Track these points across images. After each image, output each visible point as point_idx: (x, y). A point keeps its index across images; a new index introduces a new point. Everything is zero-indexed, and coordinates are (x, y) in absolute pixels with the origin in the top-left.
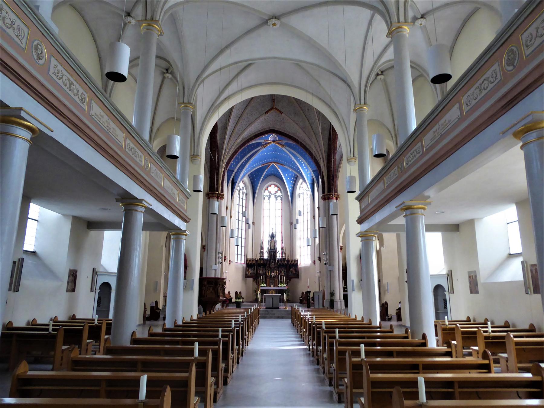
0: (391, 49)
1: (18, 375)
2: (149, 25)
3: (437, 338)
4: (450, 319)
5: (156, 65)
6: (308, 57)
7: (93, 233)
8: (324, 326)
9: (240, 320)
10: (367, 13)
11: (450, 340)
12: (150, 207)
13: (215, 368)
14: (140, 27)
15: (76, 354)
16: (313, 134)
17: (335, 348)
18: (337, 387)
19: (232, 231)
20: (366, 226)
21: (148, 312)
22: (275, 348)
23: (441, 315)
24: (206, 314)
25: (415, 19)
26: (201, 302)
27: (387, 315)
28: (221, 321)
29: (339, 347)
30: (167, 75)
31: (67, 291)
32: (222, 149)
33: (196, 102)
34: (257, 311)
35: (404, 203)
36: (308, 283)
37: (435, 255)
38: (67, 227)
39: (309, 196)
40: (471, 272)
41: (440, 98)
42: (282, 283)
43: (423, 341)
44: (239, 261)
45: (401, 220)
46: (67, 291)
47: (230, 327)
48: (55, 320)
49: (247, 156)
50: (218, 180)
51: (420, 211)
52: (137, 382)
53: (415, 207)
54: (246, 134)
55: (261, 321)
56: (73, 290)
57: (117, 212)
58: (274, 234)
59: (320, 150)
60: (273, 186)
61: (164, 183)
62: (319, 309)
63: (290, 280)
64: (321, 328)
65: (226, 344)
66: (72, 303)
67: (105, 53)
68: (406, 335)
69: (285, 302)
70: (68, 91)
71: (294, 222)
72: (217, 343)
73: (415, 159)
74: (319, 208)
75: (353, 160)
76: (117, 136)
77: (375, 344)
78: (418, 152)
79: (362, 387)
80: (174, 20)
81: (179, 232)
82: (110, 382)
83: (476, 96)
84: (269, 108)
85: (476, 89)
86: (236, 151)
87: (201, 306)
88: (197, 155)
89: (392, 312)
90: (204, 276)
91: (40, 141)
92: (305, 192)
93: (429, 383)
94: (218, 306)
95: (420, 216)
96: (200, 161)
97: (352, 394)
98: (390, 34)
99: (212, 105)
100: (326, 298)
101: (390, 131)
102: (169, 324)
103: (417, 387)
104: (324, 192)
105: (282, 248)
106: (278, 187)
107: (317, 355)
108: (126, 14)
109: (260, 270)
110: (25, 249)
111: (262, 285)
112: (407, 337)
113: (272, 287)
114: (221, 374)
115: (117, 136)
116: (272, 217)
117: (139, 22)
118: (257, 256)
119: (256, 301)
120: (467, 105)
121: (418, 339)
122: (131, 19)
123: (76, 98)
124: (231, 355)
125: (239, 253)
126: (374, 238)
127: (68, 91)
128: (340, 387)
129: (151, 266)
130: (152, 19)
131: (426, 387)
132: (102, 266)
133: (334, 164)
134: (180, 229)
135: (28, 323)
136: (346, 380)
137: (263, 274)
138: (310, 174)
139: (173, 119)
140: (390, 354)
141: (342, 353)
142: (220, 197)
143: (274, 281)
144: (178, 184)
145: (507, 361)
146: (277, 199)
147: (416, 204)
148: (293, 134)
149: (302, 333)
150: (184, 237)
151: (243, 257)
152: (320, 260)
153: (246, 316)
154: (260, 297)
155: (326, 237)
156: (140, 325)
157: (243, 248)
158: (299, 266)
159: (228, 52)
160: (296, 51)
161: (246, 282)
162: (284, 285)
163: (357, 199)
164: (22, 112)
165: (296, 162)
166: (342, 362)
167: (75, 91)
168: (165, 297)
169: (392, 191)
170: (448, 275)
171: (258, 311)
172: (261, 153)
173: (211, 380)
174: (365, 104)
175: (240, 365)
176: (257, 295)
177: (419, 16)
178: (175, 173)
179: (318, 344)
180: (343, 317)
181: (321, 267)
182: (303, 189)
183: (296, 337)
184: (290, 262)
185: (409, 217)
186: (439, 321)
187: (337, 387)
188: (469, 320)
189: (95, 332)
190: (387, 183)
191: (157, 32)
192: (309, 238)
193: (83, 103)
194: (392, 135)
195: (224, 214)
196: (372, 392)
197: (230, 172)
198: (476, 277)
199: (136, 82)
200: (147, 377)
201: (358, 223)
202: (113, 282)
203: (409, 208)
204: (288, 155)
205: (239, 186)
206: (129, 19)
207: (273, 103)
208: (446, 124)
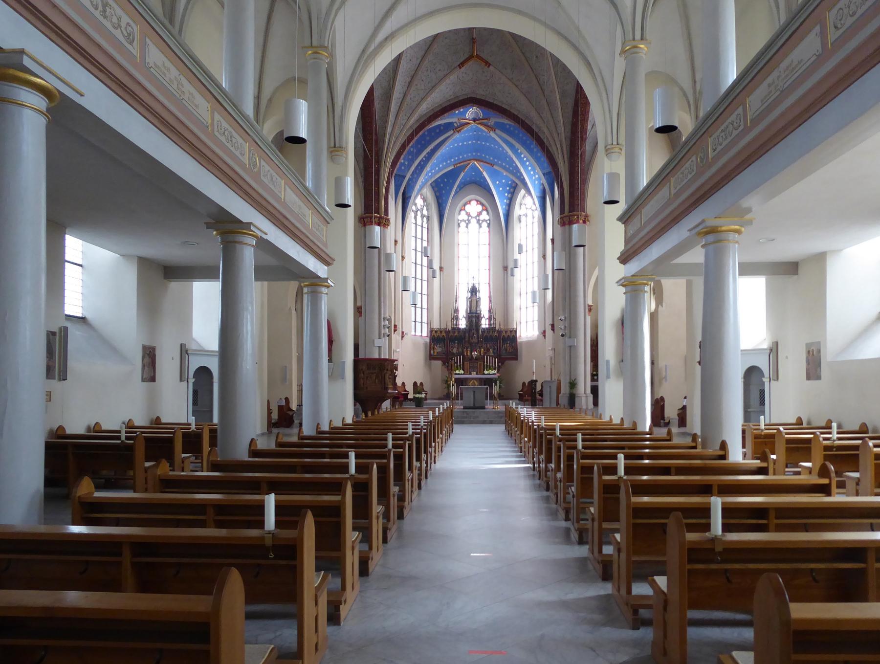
1: (79, 497)
4: (767, 422)
7: (175, 286)
8: (558, 432)
9: (422, 424)
12: (264, 236)
15: (164, 469)
18: (578, 522)
19: (405, 279)
20: (634, 267)
21: (275, 416)
22: (479, 475)
23: (753, 416)
24: (366, 416)
26: (358, 398)
27: (663, 418)
28: (393, 425)
29: (581, 461)
31: (143, 380)
33: (333, 45)
34: (449, 411)
35: (703, 221)
36: (532, 368)
37: (751, 314)
38: (130, 276)
39: (536, 219)
40: (812, 344)
41: (783, 19)
43: (722, 453)
44: (418, 333)
46: (143, 380)
47: (407, 433)
48: (130, 425)
49: (428, 150)
50: (378, 193)
51: (731, 236)
52: (260, 508)
53: (724, 228)
54: (425, 108)
55: (456, 427)
56: (153, 379)
57: (209, 248)
58: (477, 286)
60: (474, 203)
61: (287, 197)
62: (550, 408)
63: (503, 363)
65: (399, 458)
66: (152, 400)
68: (694, 444)
70: (101, 18)
71: (511, 265)
72: (385, 456)
73: (730, 139)
74: (553, 240)
75: (617, 150)
77: (641, 457)
81: (315, 282)
82: (219, 508)
84: (467, 56)
86: (409, 140)
88: (341, 147)
89: (671, 412)
90: (361, 356)
91: (64, 114)
92: (530, 213)
93: (727, 511)
94: (386, 405)
95: (731, 245)
96: (346, 158)
97: (601, 531)
99: (364, 51)
100: (563, 391)
101: (685, 95)
102: (308, 430)
104: (562, 211)
105: (490, 311)
107: (546, 476)
109: (453, 347)
110: (67, 312)
111: (457, 372)
112: (695, 448)
113: (474, 375)
114: (394, 502)
115: (197, 106)
116: (473, 258)
118: (447, 325)
119: (448, 396)
123: (117, 33)
124: (408, 474)
125: (418, 319)
126: (647, 288)
127: (101, 18)
129: (275, 341)
131: (724, 517)
132: (194, 340)
133: (583, 160)
134: (315, 276)
135: (89, 429)
136: (592, 510)
137: (459, 354)
138: (539, 178)
139: (297, 84)
140: (666, 471)
141: (587, 470)
142: (383, 222)
144: (310, 198)
145: (857, 484)
146: (480, 227)
147: (726, 224)
148: (513, 106)
149: (522, 445)
151: (425, 326)
152: (553, 329)
153: (431, 418)
155: (564, 299)
156: (263, 434)
157: (425, 312)
158: (519, 340)
161: (429, 366)
162: (494, 372)
164: (25, 57)
165: (515, 159)
167: (115, 20)
168: (300, 391)
170: (771, 350)
171: (450, 413)
172: (453, 143)
173: (377, 509)
174: (642, 39)
175: (423, 491)
176: (449, 386)
178: (304, 177)
179: (548, 460)
180: (589, 419)
182: (527, 207)
185: (711, 247)
186: (751, 424)
188: (799, 422)
189: (192, 442)
193: (131, 43)
194: (689, 106)
195: (390, 248)
196: (635, 526)
197: (400, 178)
198: (819, 351)
199: (223, 7)
201: (621, 262)
202: (214, 365)
203: (713, 230)
204: (501, 146)
205: (416, 205)
207: (473, 46)
208: (794, 69)
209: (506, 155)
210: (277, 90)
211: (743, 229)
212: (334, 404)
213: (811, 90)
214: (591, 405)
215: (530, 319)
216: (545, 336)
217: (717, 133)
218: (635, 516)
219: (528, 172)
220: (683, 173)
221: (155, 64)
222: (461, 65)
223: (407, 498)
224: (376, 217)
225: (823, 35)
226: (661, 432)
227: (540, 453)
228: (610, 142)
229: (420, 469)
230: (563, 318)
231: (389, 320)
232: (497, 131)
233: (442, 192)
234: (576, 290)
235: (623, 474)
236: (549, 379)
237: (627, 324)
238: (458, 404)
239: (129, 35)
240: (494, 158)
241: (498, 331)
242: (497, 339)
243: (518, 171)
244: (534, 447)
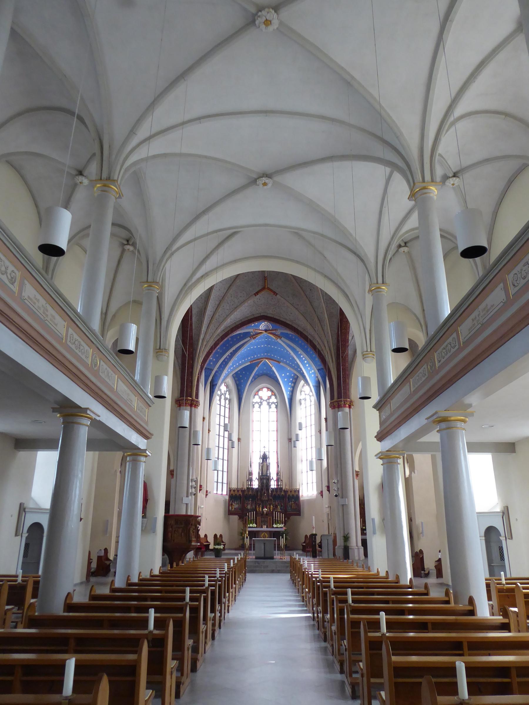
0: (415, 216)
2: (105, 186)
3: (491, 603)
4: (508, 576)
5: (113, 235)
6: (309, 224)
7: (22, 454)
8: (332, 585)
10: (381, 171)
11: (507, 607)
12: (98, 418)
13: (178, 646)
14: (94, 188)
16: (317, 321)
17: (346, 616)
18: (351, 676)
19: (208, 450)
21: (94, 565)
22: (267, 618)
23: (496, 570)
24: (171, 567)
25: (445, 178)
27: (423, 569)
28: (192, 578)
29: (351, 616)
30: (128, 247)
33: (163, 280)
34: (243, 561)
35: (436, 413)
36: (313, 523)
39: (313, 403)
41: (481, 274)
42: (278, 522)
43: (470, 608)
44: (220, 492)
45: (434, 437)
47: (204, 585)
49: (231, 350)
50: (192, 382)
51: (459, 424)
52: (61, 668)
53: (452, 418)
54: (229, 322)
55: (249, 576)
57: (54, 426)
58: (267, 454)
59: (327, 343)
60: (265, 390)
61: (119, 388)
62: (328, 559)
63: (289, 518)
64: (329, 587)
65: (195, 610)
67: (45, 218)
68: (447, 599)
69: (282, 550)
71: (294, 439)
72: (182, 610)
73: (449, 354)
76: (56, 325)
77: (402, 612)
78: (453, 345)
79: (381, 676)
80: (137, 180)
81: (135, 452)
83: (525, 274)
84: (260, 288)
85: (524, 266)
86: (216, 345)
87: (166, 556)
89: (429, 564)
90: (171, 513)
92: (308, 397)
93: (471, 670)
94: (190, 555)
96: (168, 357)
97: (369, 684)
98: (413, 196)
99: (185, 285)
100: (338, 544)
102: (119, 582)
103: (455, 676)
104: (332, 397)
105: (277, 474)
106: (272, 391)
107: (324, 627)
108: (77, 173)
111: (251, 525)
112: (448, 602)
113: (264, 528)
114: (188, 655)
115: (56, 325)
116: (264, 432)
117: (92, 183)
118: (243, 485)
119: (242, 547)
120: (514, 285)
121: (463, 606)
122: (84, 178)
124: (202, 627)
125: (220, 480)
128: (354, 676)
129: (101, 497)
130: (109, 179)
132: (33, 500)
136: (361, 664)
138: (314, 373)
140: (422, 626)
141: (355, 624)
142: (194, 404)
143: (266, 519)
144: (137, 388)
146: (270, 407)
147: (454, 415)
148: (293, 321)
149: (304, 595)
150: (143, 459)
152: (329, 490)
153: (226, 570)
154: (247, 541)
156: (82, 583)
158: (301, 499)
159: (205, 218)
160: (294, 217)
161: (228, 520)
163: (375, 407)
166: (355, 636)
169: (420, 397)
171: (243, 562)
172: (250, 346)
173: (171, 664)
174: (383, 283)
175: (216, 642)
176: (243, 538)
177: (451, 175)
179: (325, 612)
180: (361, 572)
181: (331, 501)
182: (306, 393)
183: (297, 601)
184: (293, 492)
185: (445, 431)
187: (351, 676)
190: (414, 386)
191: (114, 194)
192: (314, 460)
193: (13, 284)
196: (396, 683)
200: (76, 661)
201: (378, 440)
203: (444, 420)
204: (285, 349)
205: (220, 390)
206: (80, 178)
207: (265, 282)
208: (487, 311)
209: (289, 355)
210: (120, 308)
211: (467, 419)
212: (144, 557)
213: (502, 325)
214: (362, 557)
215: (310, 481)
216: (322, 495)
217: (440, 350)
218: (396, 675)
219: (306, 368)
220: (418, 376)
221: (29, 297)
222: (256, 294)
223: (201, 649)
224: (190, 400)
225: (506, 289)
226: (420, 582)
227: (318, 605)
228: (365, 350)
229: (214, 619)
230: (336, 481)
231: (196, 482)
232: (282, 338)
233: (241, 382)
235: (385, 631)
236: (326, 533)
237: (387, 487)
238: (250, 554)
239: (12, 278)
240: (280, 357)
241: (284, 491)
242: (284, 497)
243: (299, 366)
244: (313, 597)
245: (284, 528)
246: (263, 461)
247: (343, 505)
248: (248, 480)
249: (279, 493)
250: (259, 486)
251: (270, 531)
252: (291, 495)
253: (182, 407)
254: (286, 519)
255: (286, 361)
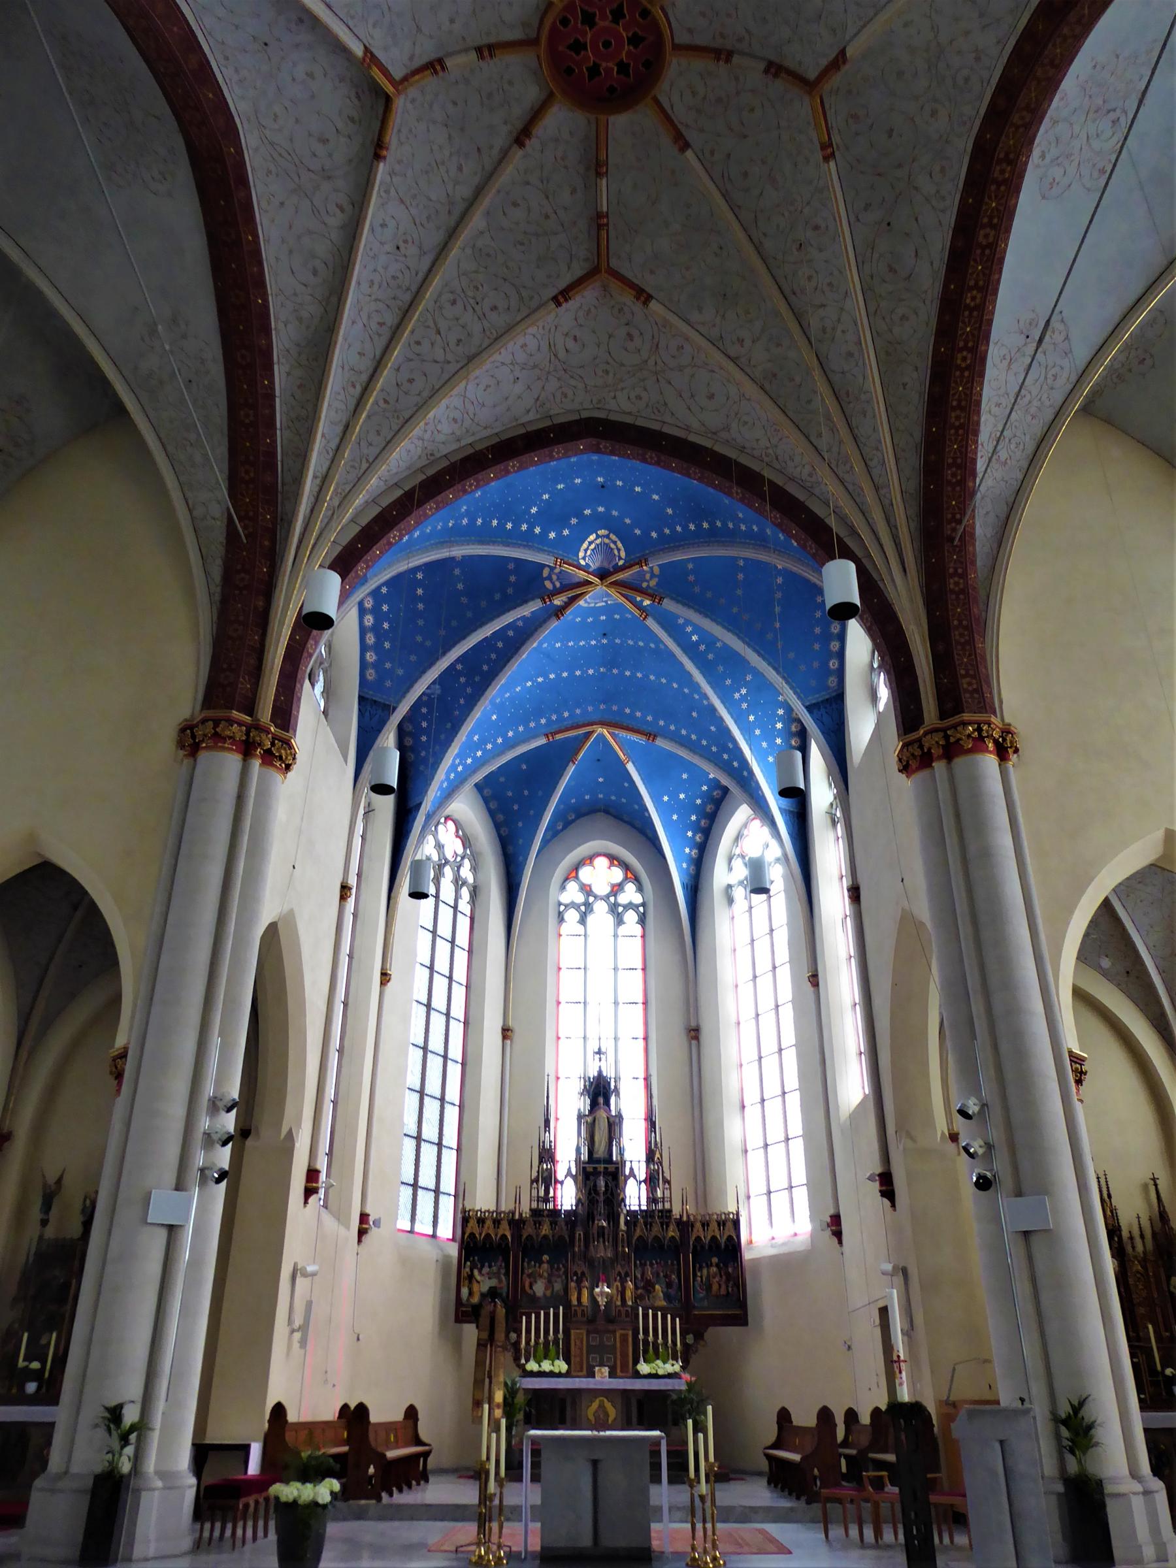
32: (298, 481)
44: (424, 1226)
60: (602, 862)
63: (699, 1336)
84: (578, 271)
105: (650, 1157)
106: (626, 867)
109: (534, 1277)
111: (546, 1366)
118: (518, 1200)
131: (668, 1457)
146: (619, 921)
158: (748, 1255)
215: (779, 1181)
216: (838, 1234)
234: (1010, 985)
242: (675, 1249)
245: (686, 1376)
246: (594, 1105)
247: (1026, 1234)
248: (536, 1180)
249: (656, 1230)
250: (579, 1201)
251: (625, 1392)
252: (706, 1240)
253: (203, 756)
254: (690, 1339)
255: (678, 730)
